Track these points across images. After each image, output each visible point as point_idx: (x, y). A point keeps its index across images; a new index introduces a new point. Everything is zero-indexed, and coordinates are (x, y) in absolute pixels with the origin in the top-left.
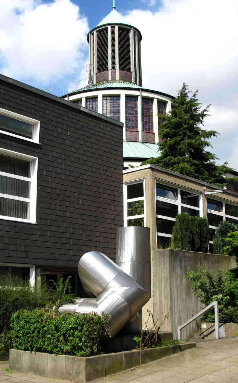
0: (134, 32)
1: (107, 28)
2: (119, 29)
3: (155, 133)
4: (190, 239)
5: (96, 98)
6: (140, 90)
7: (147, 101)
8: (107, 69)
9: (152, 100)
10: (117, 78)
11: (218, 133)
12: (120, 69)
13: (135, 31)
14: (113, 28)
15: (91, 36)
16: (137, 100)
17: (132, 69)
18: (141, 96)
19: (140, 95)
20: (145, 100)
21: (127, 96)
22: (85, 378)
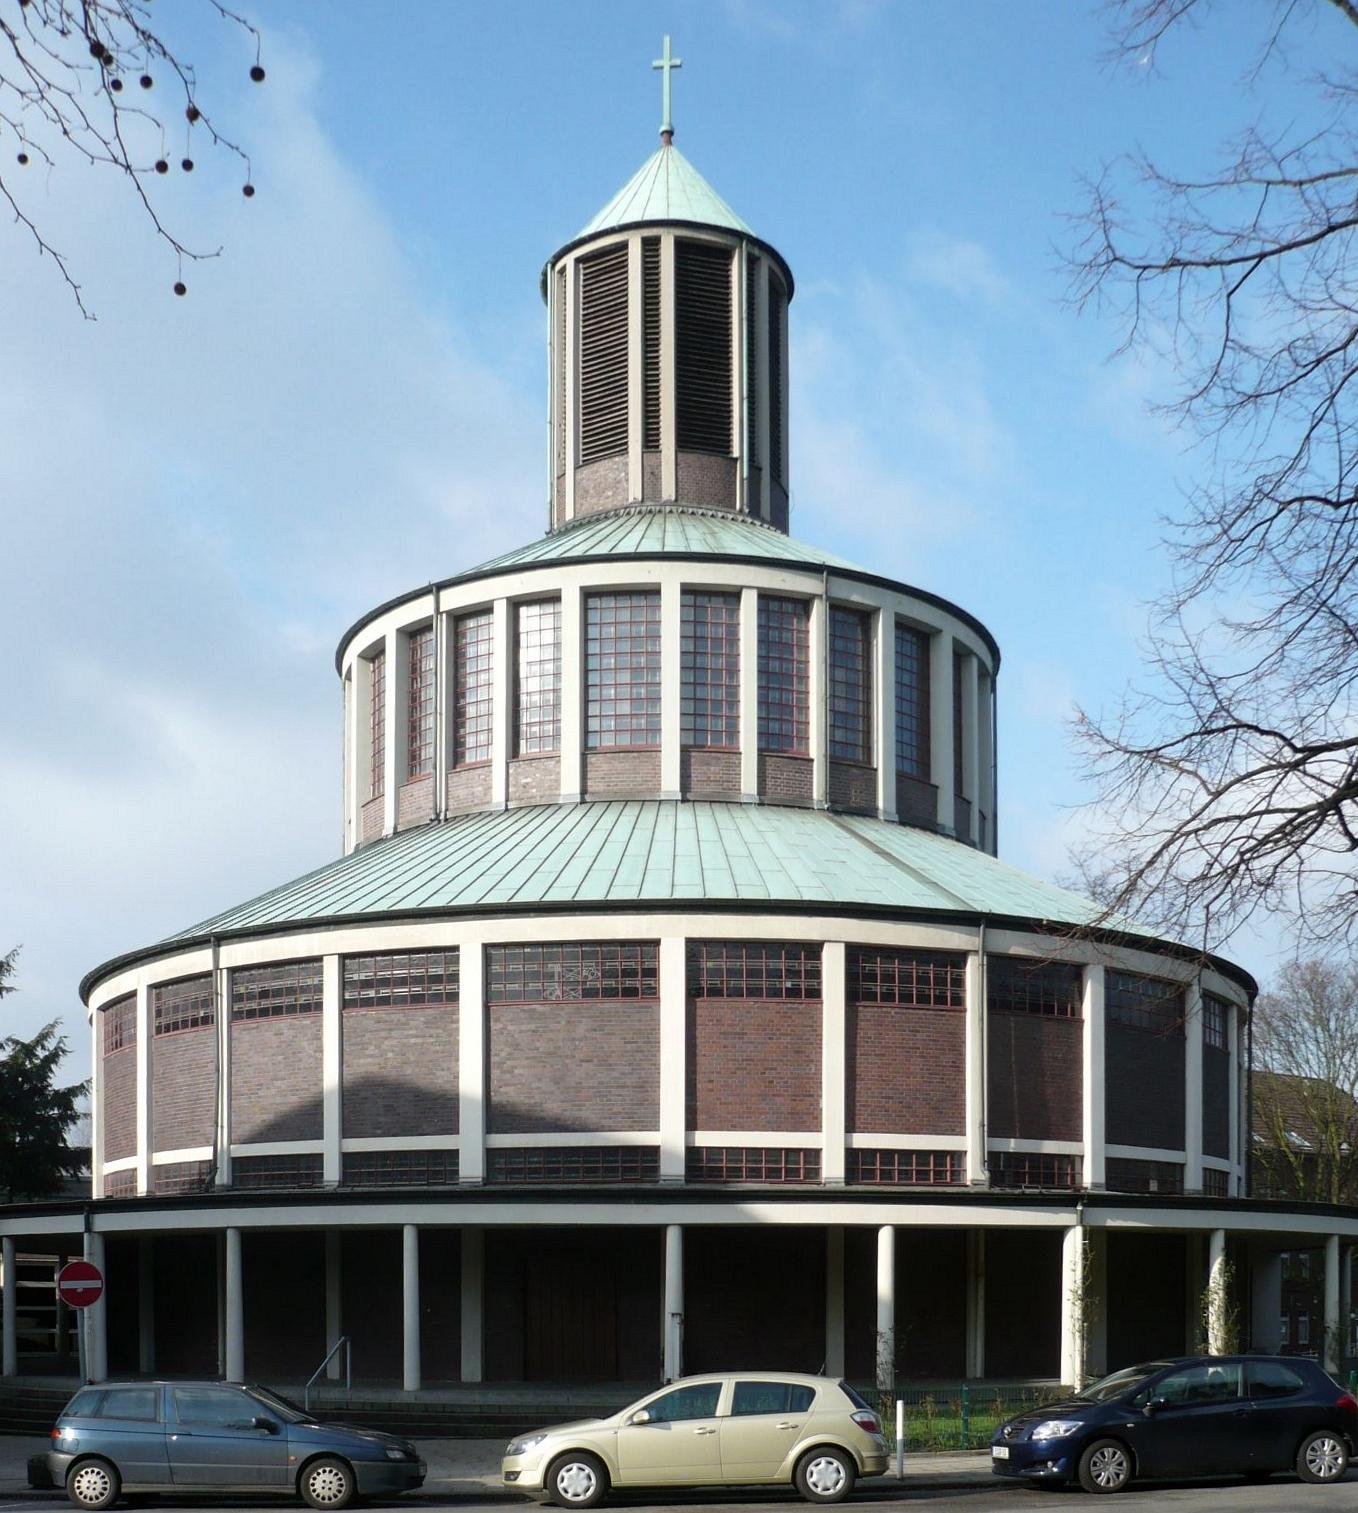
0: (752, 263)
1: (623, 246)
2: (681, 245)
3: (937, 787)
4: (1125, 1464)
5: (652, 592)
6: (822, 573)
7: (849, 623)
8: (622, 448)
9: (732, 595)
10: (668, 490)
11: (1155, 45)
12: (683, 443)
13: (756, 252)
14: (651, 246)
15: (553, 279)
16: (734, 611)
17: (738, 446)
18: (828, 598)
19: (824, 596)
20: (908, 636)
21: (766, 597)
22: (1120, 928)
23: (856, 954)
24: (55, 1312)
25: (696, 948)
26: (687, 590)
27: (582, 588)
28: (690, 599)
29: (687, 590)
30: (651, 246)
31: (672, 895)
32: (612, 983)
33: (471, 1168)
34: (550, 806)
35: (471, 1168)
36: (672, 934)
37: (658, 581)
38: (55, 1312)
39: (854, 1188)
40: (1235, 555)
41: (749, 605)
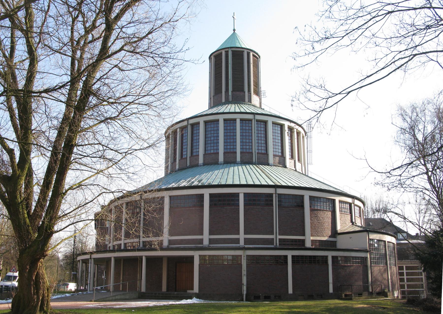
14: (227, 53)
23: (211, 195)
24: (293, 257)
25: (211, 195)
26: (225, 120)
27: (204, 121)
28: (242, 122)
29: (225, 120)
30: (227, 53)
31: (233, 182)
32: (267, 198)
33: (206, 242)
34: (197, 165)
35: (206, 242)
36: (206, 193)
37: (218, 118)
38: (293, 257)
39: (246, 246)
40: (54, 98)
41: (238, 121)
